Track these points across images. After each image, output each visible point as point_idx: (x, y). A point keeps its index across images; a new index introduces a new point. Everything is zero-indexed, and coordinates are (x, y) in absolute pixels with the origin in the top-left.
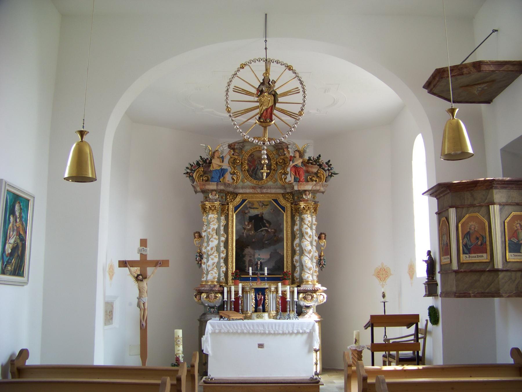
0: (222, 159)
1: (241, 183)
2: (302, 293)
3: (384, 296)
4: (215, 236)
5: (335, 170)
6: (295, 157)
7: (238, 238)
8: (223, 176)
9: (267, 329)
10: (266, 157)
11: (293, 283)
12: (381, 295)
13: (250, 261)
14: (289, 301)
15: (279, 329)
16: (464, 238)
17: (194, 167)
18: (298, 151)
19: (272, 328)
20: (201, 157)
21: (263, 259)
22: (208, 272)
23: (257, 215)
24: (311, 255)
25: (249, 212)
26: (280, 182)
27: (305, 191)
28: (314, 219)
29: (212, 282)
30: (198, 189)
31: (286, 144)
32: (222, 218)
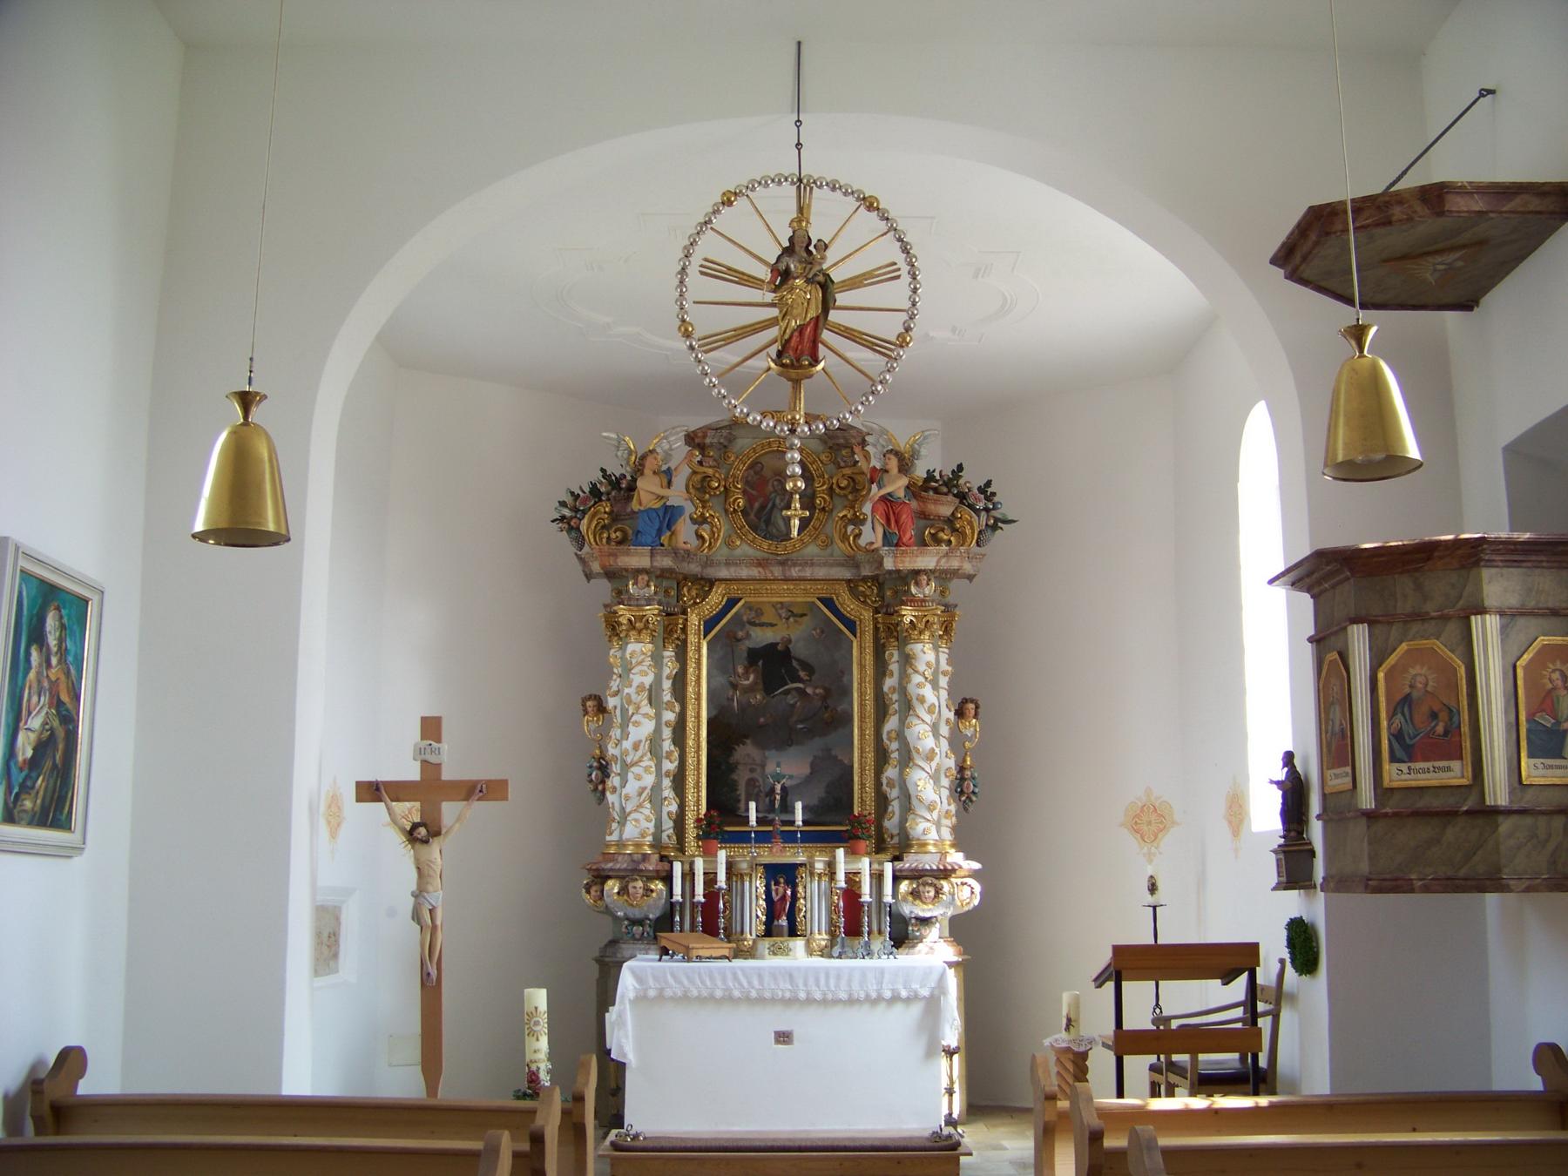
0: (668, 476)
1: (725, 550)
2: (906, 878)
3: (1153, 888)
4: (646, 709)
5: (1005, 510)
6: (887, 471)
7: (714, 713)
8: (669, 527)
9: (801, 986)
10: (798, 470)
11: (880, 848)
12: (1145, 885)
13: (751, 783)
14: (870, 904)
15: (837, 986)
16: (1394, 714)
17: (584, 502)
18: (897, 453)
19: (818, 985)
20: (603, 470)
21: (791, 777)
22: (624, 816)
23: (773, 646)
24: (934, 764)
25: (748, 636)
26: (840, 547)
27: (917, 573)
28: (943, 658)
29: (638, 845)
30: (596, 567)
31: (859, 431)
32: (666, 654)
